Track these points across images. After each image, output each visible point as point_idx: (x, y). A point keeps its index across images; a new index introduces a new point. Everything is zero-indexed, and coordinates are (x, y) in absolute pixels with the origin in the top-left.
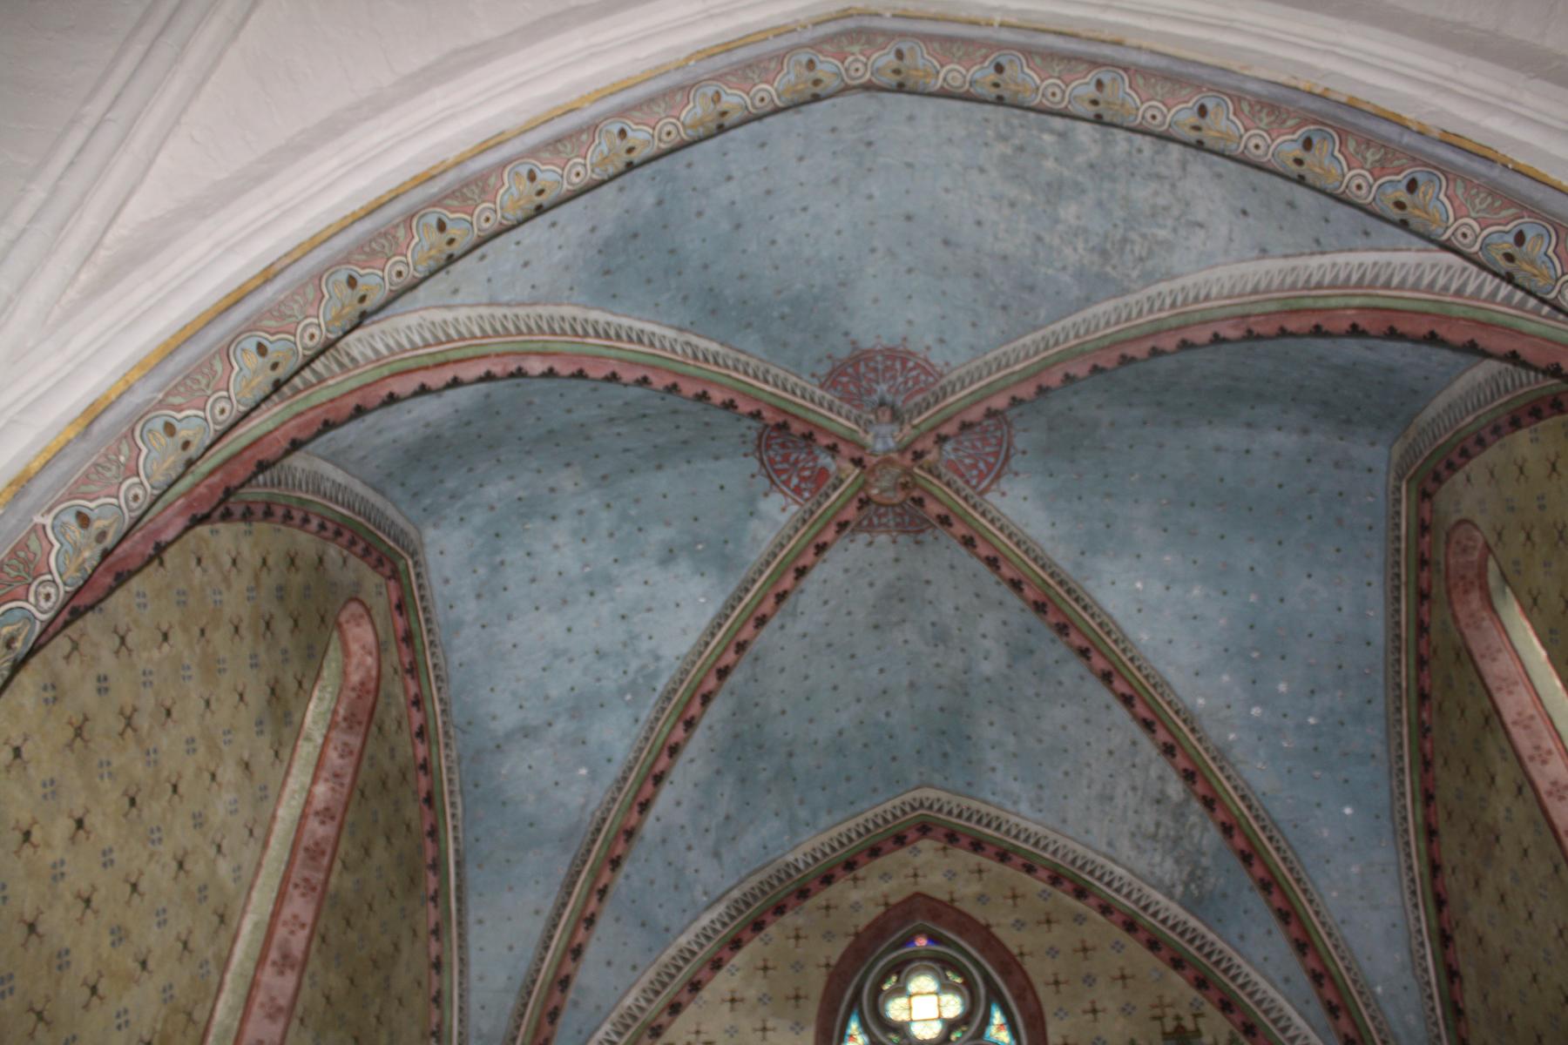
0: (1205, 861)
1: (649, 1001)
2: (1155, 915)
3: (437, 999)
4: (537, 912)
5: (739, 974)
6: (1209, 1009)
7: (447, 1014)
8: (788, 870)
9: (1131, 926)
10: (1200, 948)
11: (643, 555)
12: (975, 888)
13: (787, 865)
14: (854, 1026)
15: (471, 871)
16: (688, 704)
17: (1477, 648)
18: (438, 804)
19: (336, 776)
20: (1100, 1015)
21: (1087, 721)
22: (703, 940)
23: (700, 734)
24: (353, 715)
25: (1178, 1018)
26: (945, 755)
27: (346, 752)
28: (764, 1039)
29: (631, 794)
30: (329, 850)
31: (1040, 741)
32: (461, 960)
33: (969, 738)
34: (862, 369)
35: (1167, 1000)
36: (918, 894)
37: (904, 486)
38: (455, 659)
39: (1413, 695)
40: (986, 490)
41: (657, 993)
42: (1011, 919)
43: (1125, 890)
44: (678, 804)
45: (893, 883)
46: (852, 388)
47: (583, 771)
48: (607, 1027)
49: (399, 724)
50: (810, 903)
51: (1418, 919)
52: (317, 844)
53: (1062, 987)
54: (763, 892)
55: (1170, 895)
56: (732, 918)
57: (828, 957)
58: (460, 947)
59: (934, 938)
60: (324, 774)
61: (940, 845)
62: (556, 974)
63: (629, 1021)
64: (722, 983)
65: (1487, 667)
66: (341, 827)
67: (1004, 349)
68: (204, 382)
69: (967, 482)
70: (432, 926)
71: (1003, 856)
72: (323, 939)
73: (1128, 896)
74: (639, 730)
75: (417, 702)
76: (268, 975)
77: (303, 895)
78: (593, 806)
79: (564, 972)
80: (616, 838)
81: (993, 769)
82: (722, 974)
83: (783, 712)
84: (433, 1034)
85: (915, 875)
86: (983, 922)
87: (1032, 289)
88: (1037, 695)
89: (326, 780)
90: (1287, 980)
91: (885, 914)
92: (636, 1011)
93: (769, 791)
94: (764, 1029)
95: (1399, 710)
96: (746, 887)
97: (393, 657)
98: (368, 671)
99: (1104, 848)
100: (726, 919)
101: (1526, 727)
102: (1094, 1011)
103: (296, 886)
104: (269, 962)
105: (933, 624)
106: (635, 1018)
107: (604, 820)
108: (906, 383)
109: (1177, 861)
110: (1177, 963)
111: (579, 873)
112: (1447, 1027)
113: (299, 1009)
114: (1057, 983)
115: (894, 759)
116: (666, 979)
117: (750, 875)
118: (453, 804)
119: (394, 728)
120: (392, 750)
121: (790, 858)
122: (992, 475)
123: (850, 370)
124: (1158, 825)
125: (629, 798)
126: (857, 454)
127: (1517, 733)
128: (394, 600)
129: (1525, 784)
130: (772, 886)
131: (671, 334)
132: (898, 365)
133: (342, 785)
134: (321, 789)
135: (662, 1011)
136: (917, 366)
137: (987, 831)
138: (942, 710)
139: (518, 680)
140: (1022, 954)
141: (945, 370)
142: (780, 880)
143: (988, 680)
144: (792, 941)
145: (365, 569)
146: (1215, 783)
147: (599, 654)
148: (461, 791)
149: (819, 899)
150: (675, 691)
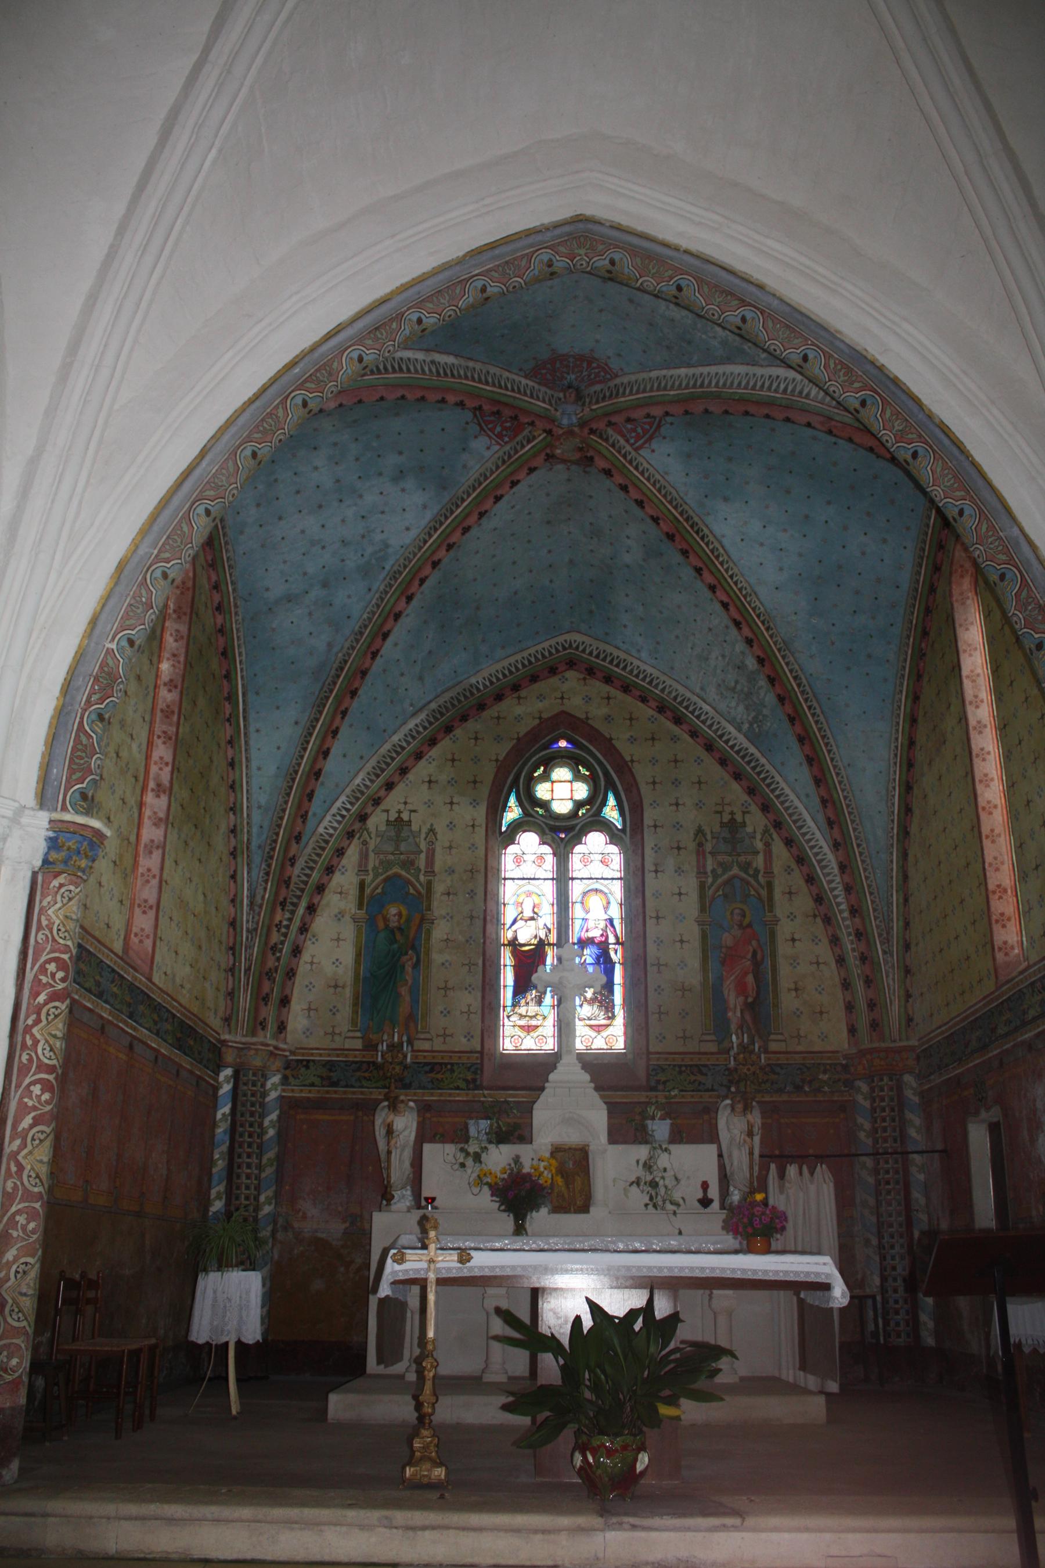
0: (765, 712)
2: (727, 742)
4: (296, 723)
5: (434, 763)
6: (754, 808)
7: (239, 796)
9: (709, 747)
10: (754, 768)
11: (380, 474)
12: (604, 711)
13: (471, 686)
14: (512, 801)
15: (251, 697)
16: (410, 583)
17: (959, 617)
18: (230, 655)
19: (174, 655)
20: (680, 807)
21: (696, 606)
22: (409, 739)
24: (180, 608)
25: (732, 813)
26: (591, 612)
28: (451, 810)
30: (176, 711)
31: (661, 612)
32: (247, 758)
33: (610, 602)
34: (558, 365)
35: (727, 801)
36: (563, 712)
37: (581, 449)
39: (920, 630)
40: (641, 447)
41: (378, 776)
42: (627, 736)
43: (709, 722)
46: (549, 376)
48: (343, 798)
50: (486, 714)
51: (895, 772)
52: (168, 706)
53: (657, 786)
54: (453, 705)
55: (739, 729)
58: (246, 750)
61: (582, 676)
63: (359, 795)
64: (422, 770)
65: (960, 632)
66: (181, 693)
67: (664, 372)
68: (179, 540)
69: (627, 441)
70: (228, 738)
71: (626, 689)
72: (178, 771)
73: (710, 727)
75: (216, 587)
77: (164, 743)
79: (318, 767)
81: (625, 626)
82: (423, 763)
83: (475, 580)
84: (231, 809)
85: (562, 698)
87: (689, 343)
88: (662, 582)
89: (168, 659)
90: (807, 796)
91: (539, 725)
92: (363, 788)
93: (461, 633)
94: (452, 803)
95: (908, 637)
96: (441, 701)
99: (698, 690)
101: (974, 681)
102: (677, 804)
103: (159, 737)
106: (363, 793)
107: (346, 662)
108: (589, 376)
109: (747, 708)
110: (737, 776)
112: (898, 840)
114: (654, 783)
115: (553, 612)
116: (384, 766)
117: (443, 692)
121: (473, 681)
122: (647, 436)
123: (549, 366)
124: (737, 682)
126: (548, 427)
127: (967, 684)
129: (963, 719)
130: (459, 701)
131: (420, 356)
132: (585, 365)
133: (179, 662)
135: (381, 788)
136: (598, 367)
138: (592, 581)
139: (285, 562)
140: (632, 761)
141: (620, 373)
143: (628, 566)
146: (778, 667)
147: (344, 542)
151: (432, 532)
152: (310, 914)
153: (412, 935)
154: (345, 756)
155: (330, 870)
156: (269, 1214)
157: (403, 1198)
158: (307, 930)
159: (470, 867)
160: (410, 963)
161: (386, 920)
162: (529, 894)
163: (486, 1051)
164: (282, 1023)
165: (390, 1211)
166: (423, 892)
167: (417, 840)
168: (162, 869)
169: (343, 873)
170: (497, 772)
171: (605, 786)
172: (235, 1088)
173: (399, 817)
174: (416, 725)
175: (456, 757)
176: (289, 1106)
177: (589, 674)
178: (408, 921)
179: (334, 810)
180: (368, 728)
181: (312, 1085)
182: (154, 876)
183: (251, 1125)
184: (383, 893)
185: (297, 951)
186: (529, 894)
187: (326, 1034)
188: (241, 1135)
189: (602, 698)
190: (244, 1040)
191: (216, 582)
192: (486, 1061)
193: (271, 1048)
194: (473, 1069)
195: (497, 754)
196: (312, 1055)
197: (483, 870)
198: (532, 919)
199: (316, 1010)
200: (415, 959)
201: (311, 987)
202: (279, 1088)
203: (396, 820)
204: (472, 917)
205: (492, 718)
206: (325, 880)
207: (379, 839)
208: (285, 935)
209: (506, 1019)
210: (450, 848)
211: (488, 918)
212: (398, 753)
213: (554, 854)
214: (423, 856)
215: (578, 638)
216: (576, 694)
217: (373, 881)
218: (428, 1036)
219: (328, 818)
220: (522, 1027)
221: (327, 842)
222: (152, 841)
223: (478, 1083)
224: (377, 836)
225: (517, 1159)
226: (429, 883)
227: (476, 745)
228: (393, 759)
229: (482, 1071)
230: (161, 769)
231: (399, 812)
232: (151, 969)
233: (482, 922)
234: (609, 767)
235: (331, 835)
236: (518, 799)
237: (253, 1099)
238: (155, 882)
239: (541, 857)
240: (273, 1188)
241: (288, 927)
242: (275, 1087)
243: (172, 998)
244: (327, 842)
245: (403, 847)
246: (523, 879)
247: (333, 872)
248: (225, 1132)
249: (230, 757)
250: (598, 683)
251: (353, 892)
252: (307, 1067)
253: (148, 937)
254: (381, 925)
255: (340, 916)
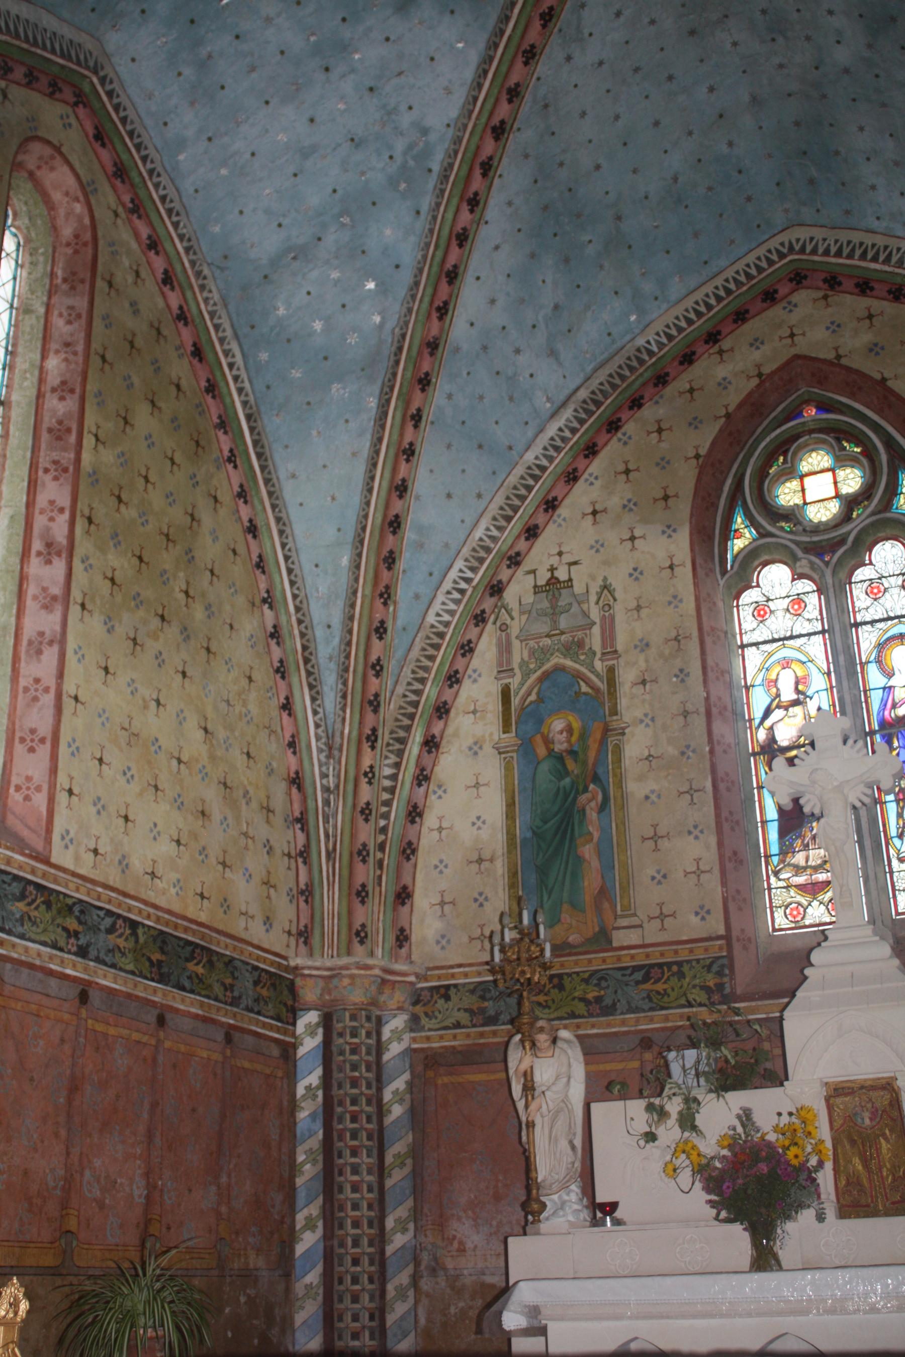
1: (500, 529)
3: (260, 565)
4: (354, 454)
5: (598, 483)
8: (638, 357)
12: (867, 337)
14: (739, 521)
18: (210, 356)
19: (67, 345)
22: (552, 452)
23: (494, 209)
24: (74, 274)
26: (812, 182)
27: (72, 316)
28: (633, 548)
29: (427, 299)
33: (837, 153)
36: (797, 357)
38: (187, 186)
41: (508, 519)
44: (493, 301)
45: (766, 349)
47: (371, 285)
48: (460, 564)
49: (137, 273)
50: (669, 390)
52: (60, 422)
54: (614, 387)
56: (582, 422)
57: (696, 448)
59: (824, 406)
60: (54, 346)
61: (821, 294)
62: (385, 516)
63: (482, 554)
64: (580, 497)
70: (236, 489)
74: (422, 224)
75: (153, 245)
76: (35, 566)
77: (56, 478)
78: (390, 325)
79: (393, 512)
80: (420, 353)
81: (873, 188)
82: (580, 485)
83: (598, 167)
85: (792, 335)
86: (878, 377)
89: (57, 352)
92: (488, 542)
93: (601, 267)
94: (633, 538)
96: (594, 384)
97: (107, 197)
98: (80, 218)
100: (575, 424)
103: (46, 471)
104: (33, 552)
105: (764, 12)
106: (488, 550)
107: (403, 336)
111: (388, 401)
113: (76, 595)
115: (749, 199)
116: (517, 502)
117: (595, 370)
118: (226, 353)
119: (130, 279)
120: (133, 304)
121: (641, 342)
125: (425, 305)
128: (91, 131)
130: (623, 378)
133: (75, 353)
134: (53, 363)
135: (518, 537)
137: (873, 266)
138: (797, 124)
142: (632, 369)
143: (846, 71)
144: (655, 435)
145: (36, 99)
148: (236, 336)
149: (682, 383)
150: (451, 166)
151: (482, 81)
152: (429, 752)
153: (591, 761)
154: (449, 496)
155: (453, 679)
156: (403, 1247)
157: (564, 1207)
158: (427, 778)
159: (673, 634)
160: (593, 804)
161: (548, 742)
162: (786, 664)
163: (735, 933)
164: (402, 930)
165: (538, 1233)
166: (603, 686)
167: (585, 607)
168: (60, 675)
169: (475, 681)
170: (700, 475)
171: (891, 462)
172: (327, 1043)
173: (552, 577)
174: (560, 430)
175: (631, 467)
176: (426, 1063)
177: (832, 288)
178: (583, 736)
179: (447, 585)
180: (480, 447)
181: (458, 1025)
182: (47, 690)
183: (354, 1102)
184: (540, 700)
185: (415, 813)
186: (786, 664)
187: (471, 939)
188: (341, 1120)
189: (859, 320)
190: (329, 963)
191: (149, 237)
192: (737, 947)
193: (377, 972)
194: (715, 968)
195: (696, 448)
196: (453, 976)
197: (695, 633)
198: (795, 703)
199: (453, 903)
200: (600, 797)
201: (441, 867)
202: (407, 1037)
203: (548, 583)
204: (686, 714)
205: (681, 393)
206: (448, 695)
207: (524, 618)
208: (392, 790)
209: (773, 879)
210: (638, 608)
211: (714, 710)
212: (536, 478)
213: (820, 591)
214: (596, 630)
215: (803, 234)
216: (814, 325)
217: (522, 684)
218: (634, 921)
219: (441, 597)
220: (801, 888)
221: (441, 635)
222: (41, 634)
223: (727, 990)
224: (522, 613)
225: (746, 1117)
226: (611, 670)
227: (660, 441)
228: (529, 489)
229: (731, 967)
230: (52, 519)
231: (552, 569)
232: (48, 840)
233: (703, 718)
234: (890, 429)
235: (447, 624)
236: (749, 516)
237: (355, 1057)
238: (48, 699)
239: (798, 601)
240: (410, 1203)
241: (394, 777)
242: (397, 1035)
243: (126, 895)
244: (441, 635)
245: (564, 622)
246: (774, 640)
247: (458, 681)
248: (313, 1116)
249: (245, 519)
250: (848, 298)
251: (494, 706)
252: (447, 998)
253: (38, 789)
254: (542, 751)
255: (475, 749)
